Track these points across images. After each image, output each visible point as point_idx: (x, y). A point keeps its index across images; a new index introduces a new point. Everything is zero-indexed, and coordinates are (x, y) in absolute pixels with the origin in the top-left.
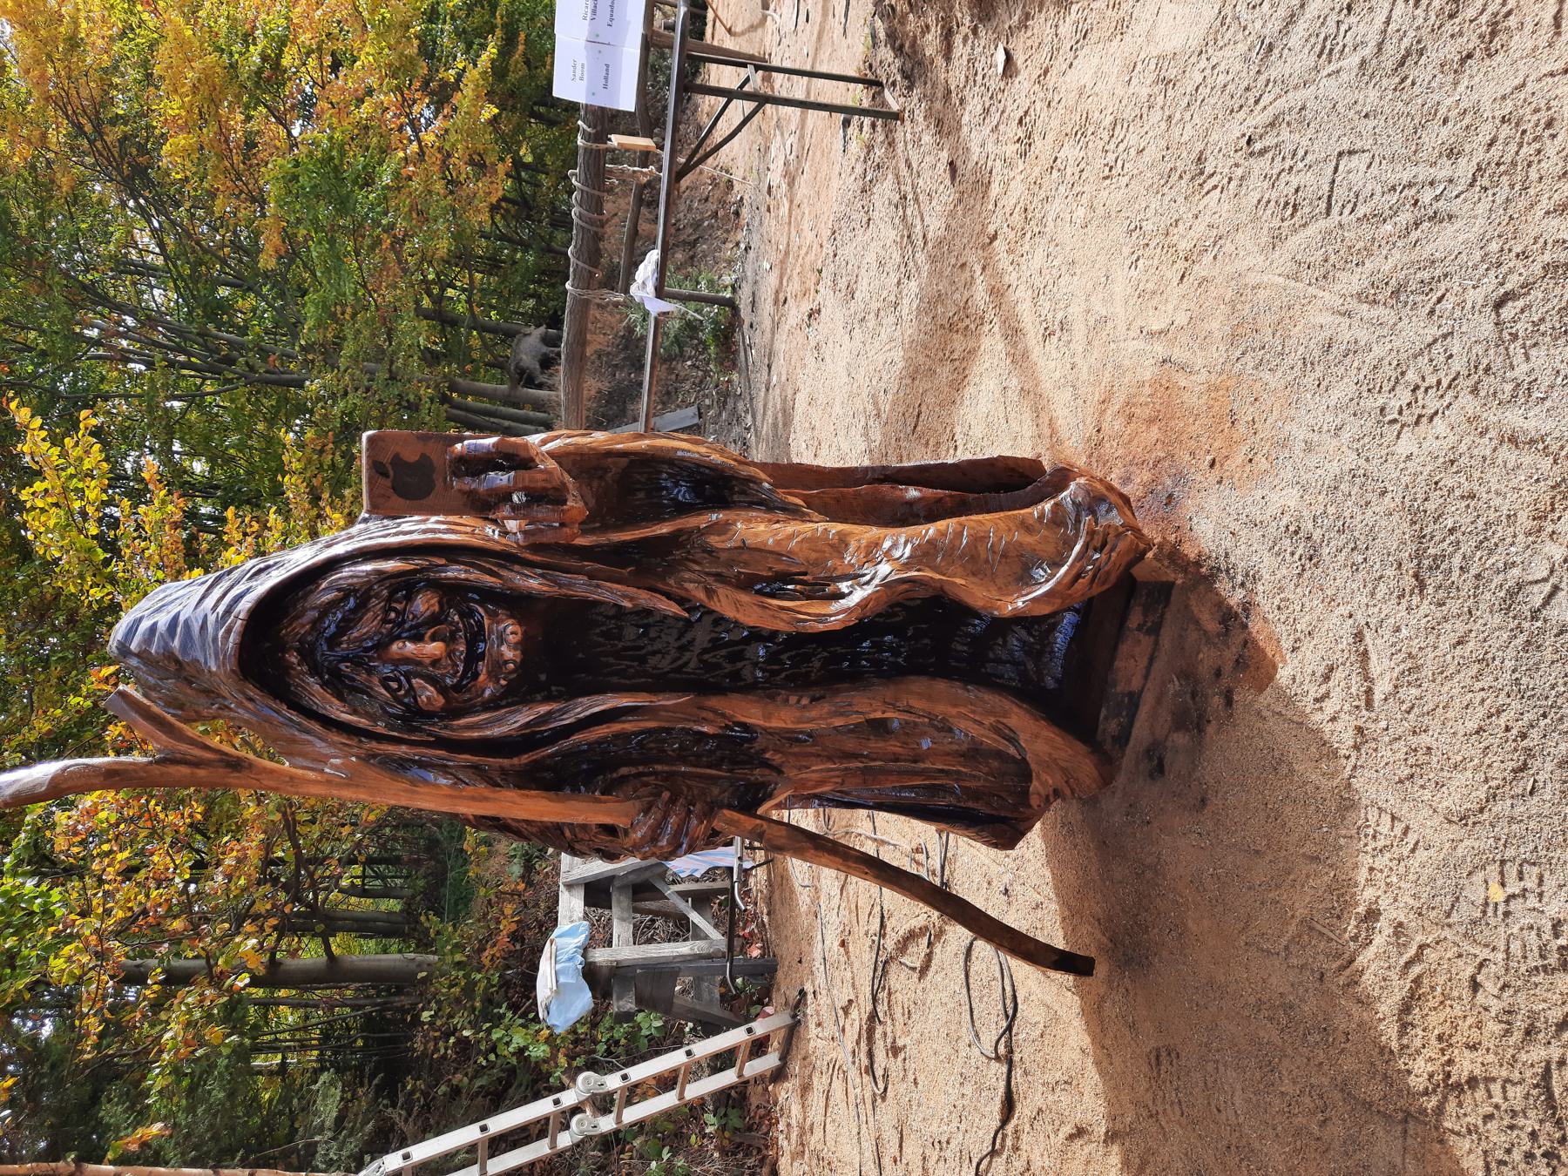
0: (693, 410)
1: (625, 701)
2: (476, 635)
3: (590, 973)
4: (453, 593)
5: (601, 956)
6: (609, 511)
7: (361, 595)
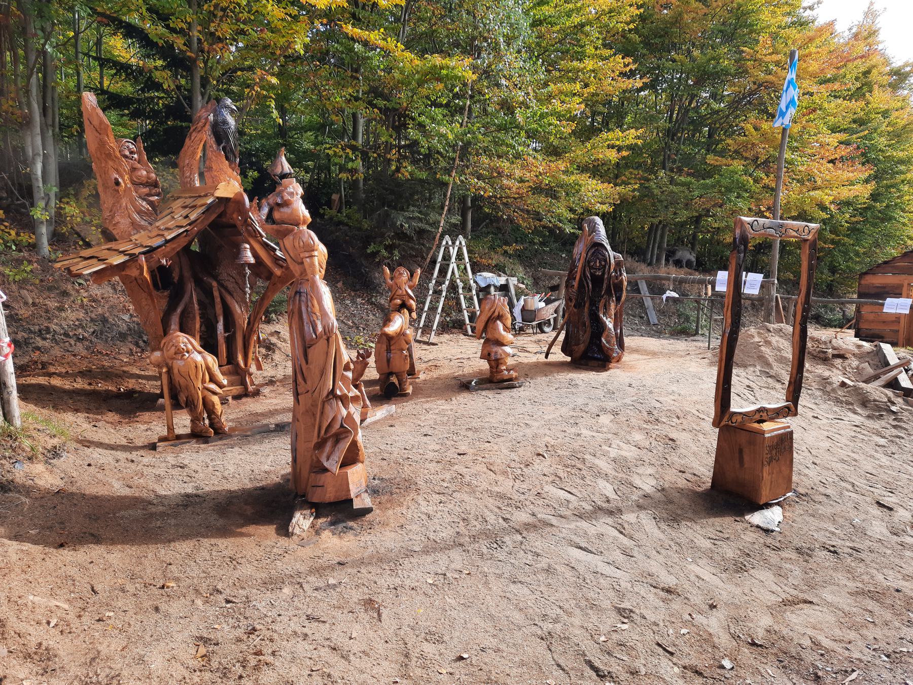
0: (656, 322)
3: (489, 286)
4: (605, 266)
5: (492, 289)
6: (615, 286)
7: (604, 256)
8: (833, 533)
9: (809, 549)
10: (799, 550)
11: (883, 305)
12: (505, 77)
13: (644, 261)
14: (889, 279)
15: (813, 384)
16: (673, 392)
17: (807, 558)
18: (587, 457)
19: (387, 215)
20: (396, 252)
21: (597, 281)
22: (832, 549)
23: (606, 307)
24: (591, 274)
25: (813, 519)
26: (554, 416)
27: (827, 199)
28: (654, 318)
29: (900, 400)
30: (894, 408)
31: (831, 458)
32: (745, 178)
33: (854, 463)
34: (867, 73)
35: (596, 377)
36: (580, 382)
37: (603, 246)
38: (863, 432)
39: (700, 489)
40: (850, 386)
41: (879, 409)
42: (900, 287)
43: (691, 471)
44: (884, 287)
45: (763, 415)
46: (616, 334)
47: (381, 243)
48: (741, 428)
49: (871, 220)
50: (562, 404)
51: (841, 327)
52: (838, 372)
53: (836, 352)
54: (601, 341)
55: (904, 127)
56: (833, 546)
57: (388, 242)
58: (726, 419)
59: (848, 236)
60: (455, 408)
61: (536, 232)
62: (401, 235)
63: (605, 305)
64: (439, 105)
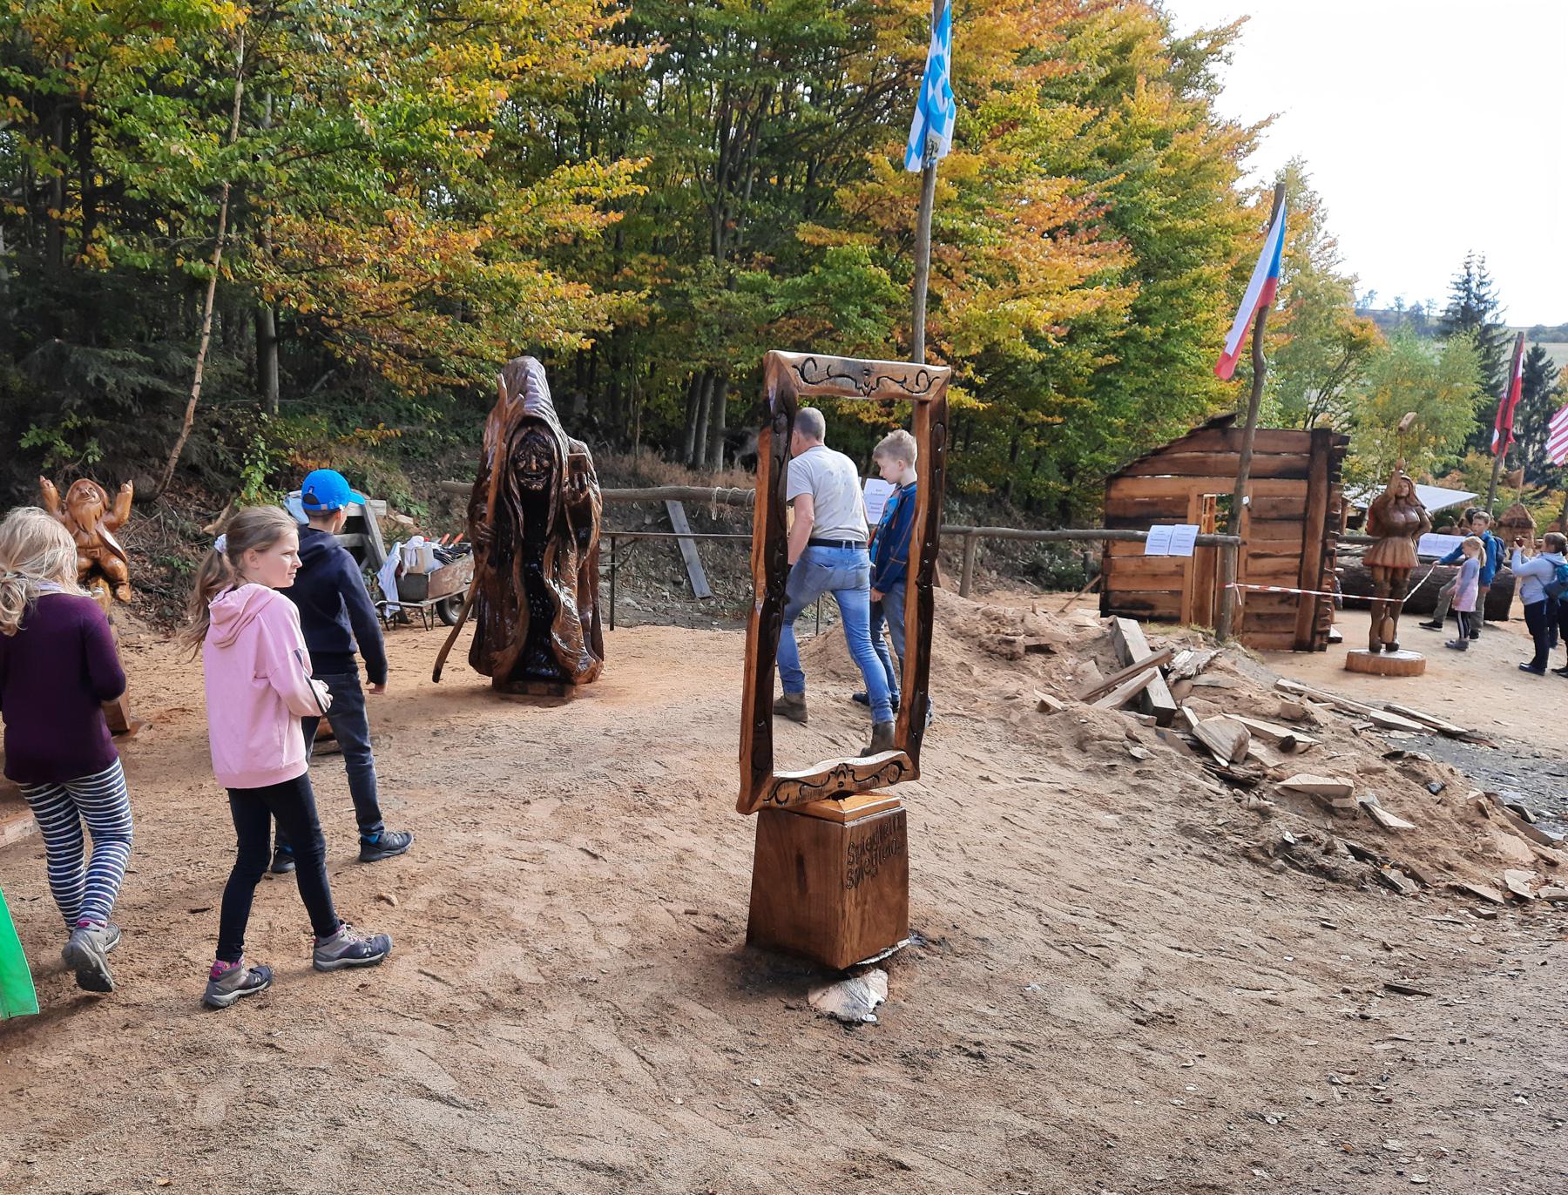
0: (708, 592)
1: (521, 515)
2: (538, 478)
4: (549, 470)
6: (573, 511)
7: (547, 446)
8: (983, 1017)
9: (929, 1054)
10: (907, 1059)
11: (1143, 540)
12: (322, 25)
13: (681, 459)
14: (1165, 485)
15: (986, 710)
16: (696, 742)
17: (921, 1072)
18: (488, 895)
19: (61, 356)
20: (93, 446)
21: (536, 503)
22: (975, 1049)
23: (560, 560)
24: (520, 487)
25: (946, 990)
26: (428, 809)
27: (1041, 320)
28: (702, 585)
29: (1150, 734)
30: (1137, 751)
31: (1004, 861)
32: (873, 270)
33: (1048, 868)
34: (1124, 49)
35: (539, 717)
36: (500, 732)
37: (543, 423)
38: (1075, 803)
39: (728, 948)
40: (1056, 711)
41: (1108, 753)
42: (1183, 501)
43: (709, 909)
44: (1152, 504)
45: (843, 783)
46: (584, 621)
47: (55, 424)
48: (800, 812)
49: (1137, 363)
50: (451, 781)
51: (1079, 590)
52: (1036, 682)
53: (1032, 641)
54: (550, 637)
55: (1198, 167)
56: (978, 1044)
57: (73, 422)
58: (764, 795)
59: (1089, 395)
60: (204, 804)
61: (431, 399)
62: (101, 404)
63: (556, 557)
64: (172, 92)
